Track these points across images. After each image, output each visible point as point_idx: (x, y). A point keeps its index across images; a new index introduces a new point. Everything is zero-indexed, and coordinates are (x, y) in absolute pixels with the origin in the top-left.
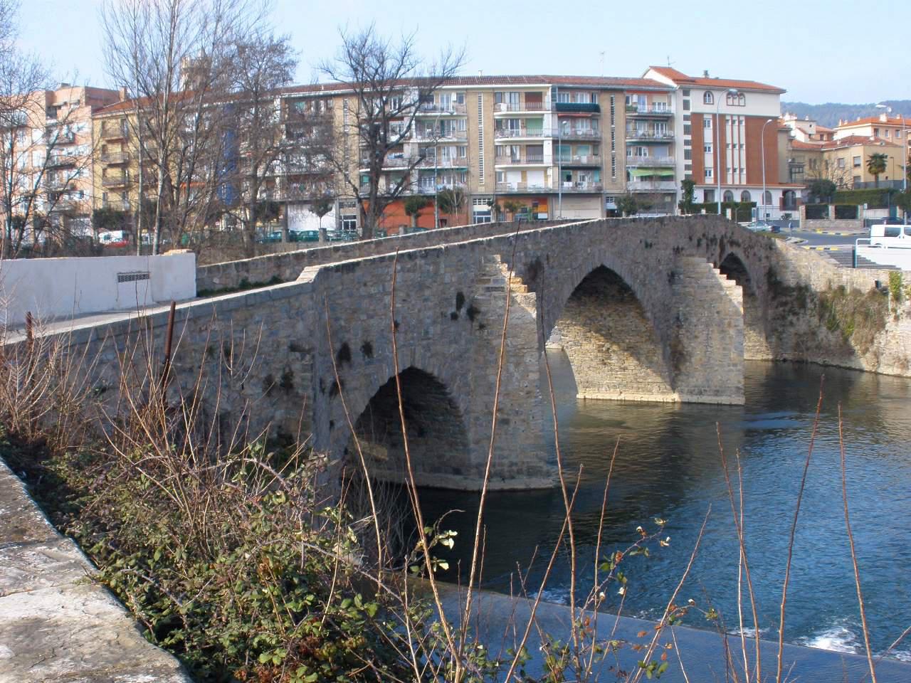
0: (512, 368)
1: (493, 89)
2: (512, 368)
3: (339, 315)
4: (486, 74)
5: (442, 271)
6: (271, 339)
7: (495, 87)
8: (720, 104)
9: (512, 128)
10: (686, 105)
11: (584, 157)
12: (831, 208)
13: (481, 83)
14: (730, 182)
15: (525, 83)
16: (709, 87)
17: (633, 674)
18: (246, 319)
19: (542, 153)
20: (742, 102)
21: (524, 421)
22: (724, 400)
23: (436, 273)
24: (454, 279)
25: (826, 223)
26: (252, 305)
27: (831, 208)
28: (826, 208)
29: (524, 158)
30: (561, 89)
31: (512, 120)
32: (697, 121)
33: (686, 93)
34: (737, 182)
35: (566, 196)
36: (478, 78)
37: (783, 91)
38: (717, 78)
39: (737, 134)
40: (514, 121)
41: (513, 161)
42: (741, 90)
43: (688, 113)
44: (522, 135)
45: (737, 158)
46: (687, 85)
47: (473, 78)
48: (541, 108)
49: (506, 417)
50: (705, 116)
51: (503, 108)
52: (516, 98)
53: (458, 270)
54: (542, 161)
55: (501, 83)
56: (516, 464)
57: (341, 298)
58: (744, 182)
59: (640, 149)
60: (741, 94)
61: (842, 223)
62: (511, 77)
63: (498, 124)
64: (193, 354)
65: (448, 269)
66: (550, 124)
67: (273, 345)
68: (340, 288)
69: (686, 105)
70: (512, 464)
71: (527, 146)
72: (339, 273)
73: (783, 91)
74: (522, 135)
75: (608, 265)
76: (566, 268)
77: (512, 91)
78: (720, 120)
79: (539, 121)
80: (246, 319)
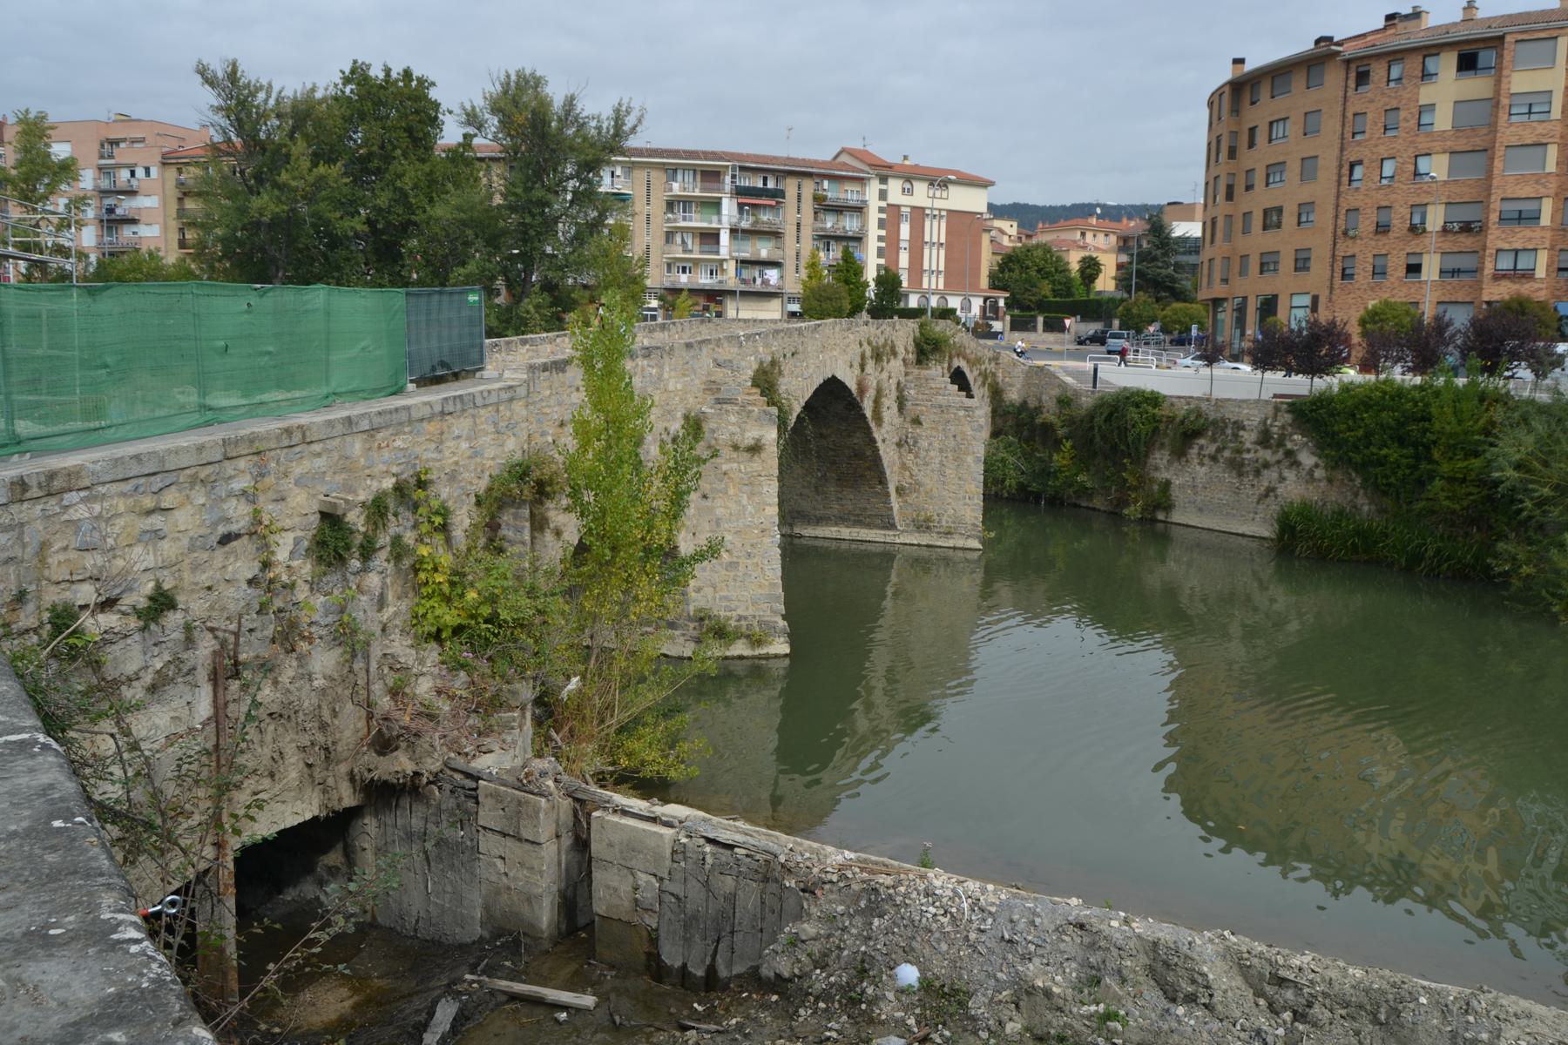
0: (745, 501)
1: (664, 164)
2: (745, 501)
3: (546, 429)
4: (654, 146)
5: (666, 376)
6: (473, 461)
7: (670, 163)
8: (921, 195)
9: (684, 212)
10: (883, 195)
11: (764, 250)
12: (1040, 319)
13: (650, 156)
14: (925, 285)
15: (700, 159)
16: (910, 176)
17: (292, 402)
18: (442, 433)
19: (718, 242)
20: (944, 195)
21: (757, 564)
22: (960, 542)
23: (660, 378)
24: (679, 386)
25: (1032, 336)
26: (450, 413)
27: (1040, 319)
28: (1034, 319)
29: (697, 248)
30: (742, 169)
31: (684, 202)
32: (892, 214)
33: (883, 180)
34: (933, 286)
35: (744, 294)
36: (647, 150)
37: (992, 184)
38: (916, 166)
39: (936, 231)
40: (686, 203)
41: (685, 251)
42: (939, 180)
43: (883, 204)
44: (698, 221)
45: (935, 259)
46: (885, 172)
47: (641, 150)
48: (719, 191)
49: (735, 560)
50: (903, 209)
51: (676, 187)
52: (689, 177)
53: (684, 375)
54: (717, 253)
55: (674, 158)
56: (746, 618)
57: (549, 406)
58: (941, 286)
59: (828, 244)
60: (945, 184)
61: (1051, 337)
62: (685, 152)
63: (670, 205)
64: (368, 482)
65: (673, 374)
66: (729, 207)
67: (476, 469)
68: (548, 392)
69: (883, 195)
70: (740, 618)
71: (701, 234)
72: (547, 373)
73: (992, 184)
74: (698, 221)
75: (840, 376)
76: (797, 377)
77: (685, 168)
78: (919, 214)
79: (716, 205)
80: (442, 433)
